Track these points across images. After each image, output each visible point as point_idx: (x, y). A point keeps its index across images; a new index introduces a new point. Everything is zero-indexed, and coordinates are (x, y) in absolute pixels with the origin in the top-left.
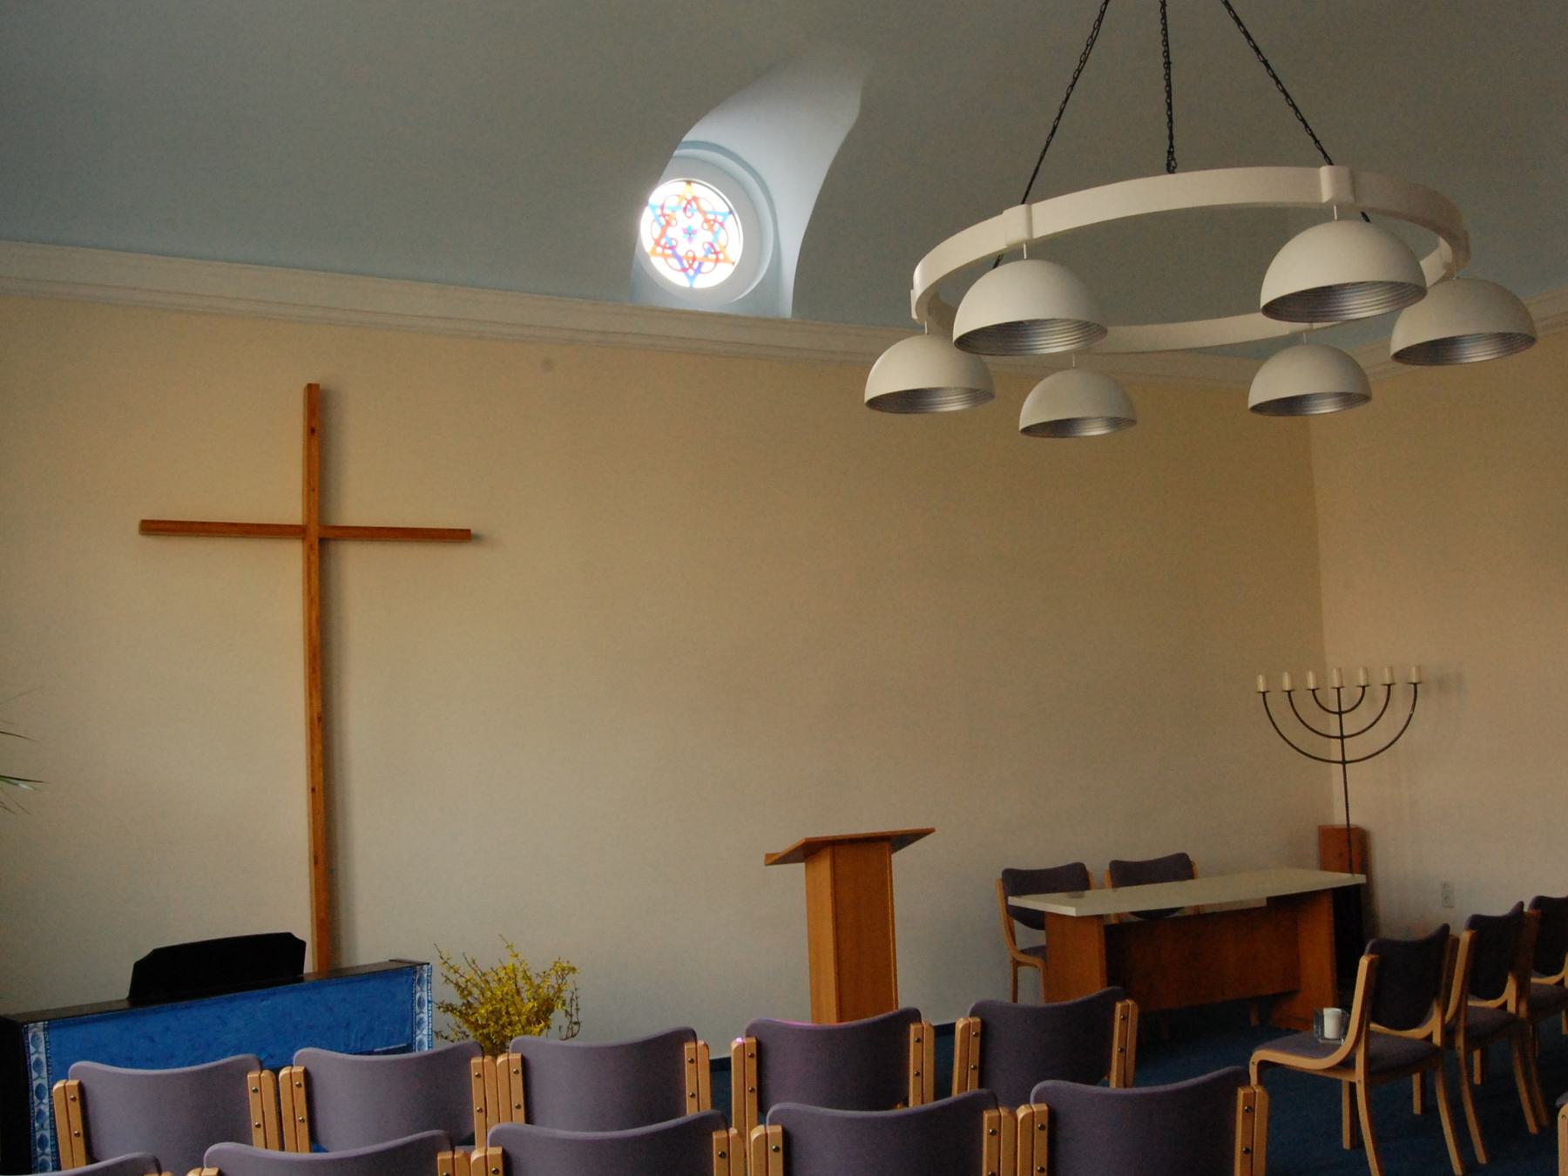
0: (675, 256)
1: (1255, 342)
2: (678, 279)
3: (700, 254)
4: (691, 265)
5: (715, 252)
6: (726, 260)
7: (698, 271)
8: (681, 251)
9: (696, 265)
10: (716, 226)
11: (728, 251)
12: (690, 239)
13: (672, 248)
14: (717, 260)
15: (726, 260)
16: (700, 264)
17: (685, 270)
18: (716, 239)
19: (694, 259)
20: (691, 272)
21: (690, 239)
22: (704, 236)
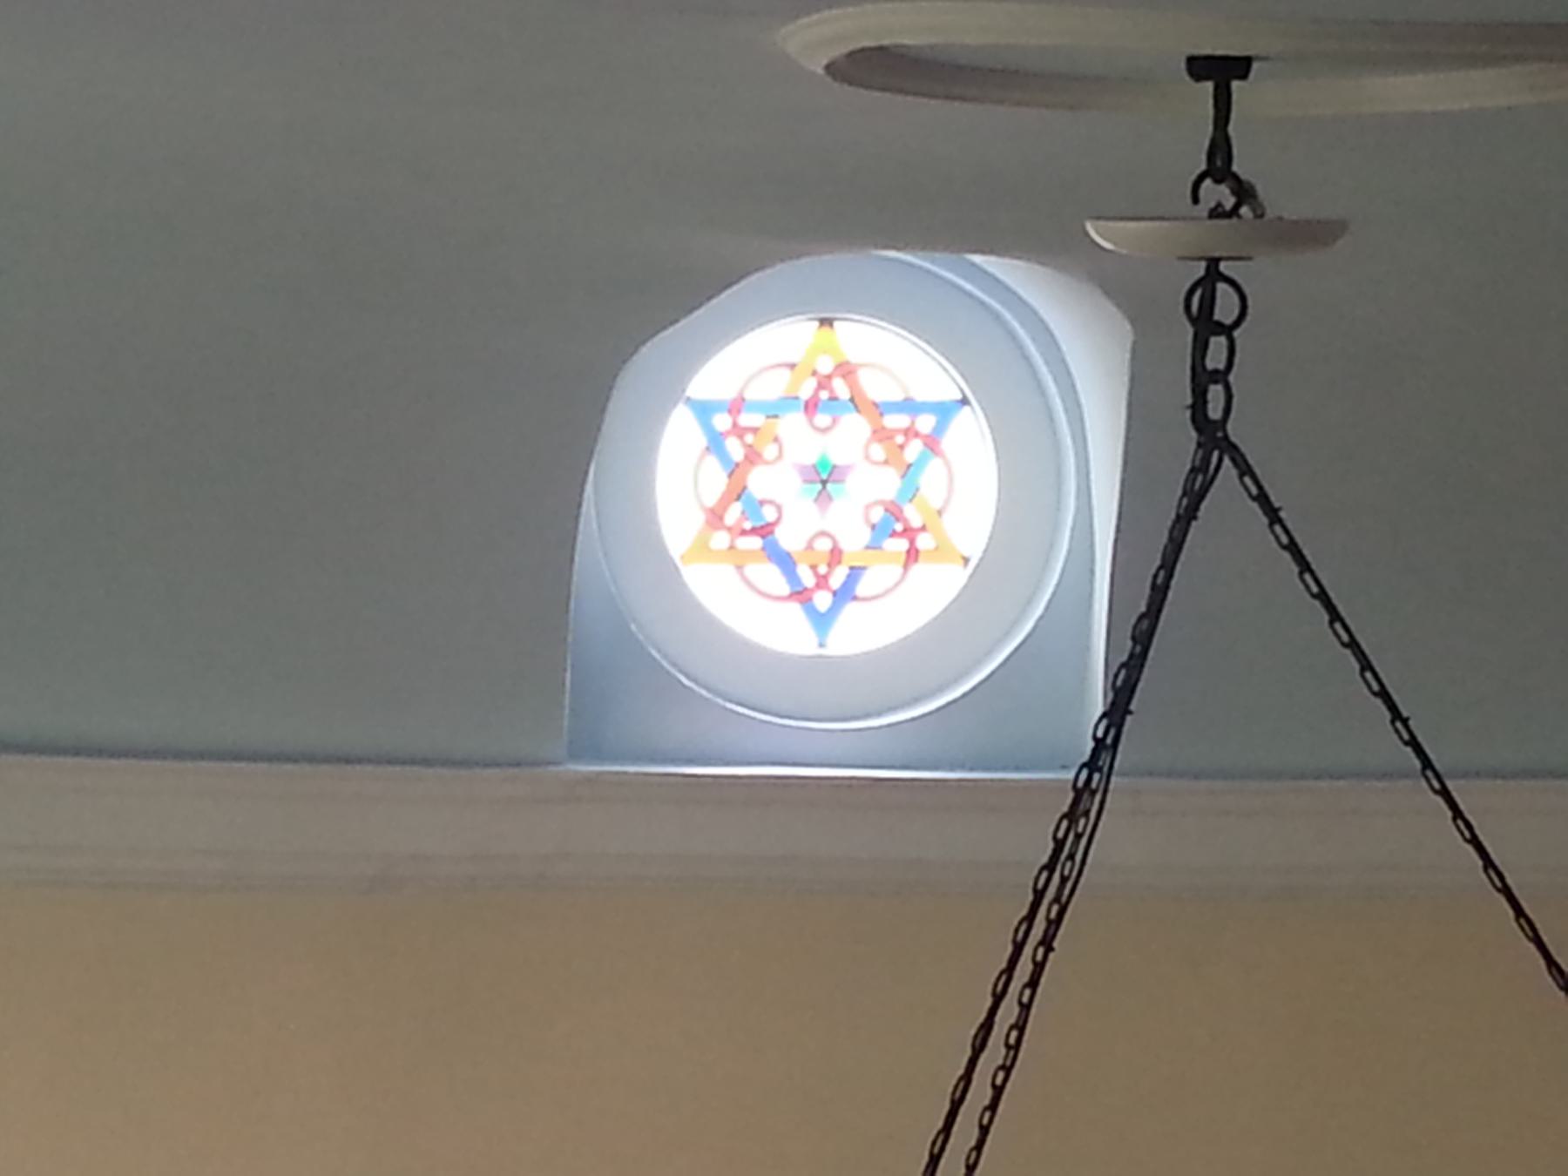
0: (736, 472)
1: (935, 619)
2: (933, 590)
3: (854, 539)
4: (824, 585)
5: (898, 528)
6: (942, 551)
7: (845, 594)
8: (789, 538)
9: (838, 578)
10: (914, 449)
11: (949, 523)
12: (823, 499)
13: (764, 531)
14: (912, 555)
15: (942, 551)
16: (855, 572)
17: (801, 595)
18: (913, 493)
19: (835, 555)
20: (720, 540)
21: (823, 499)
22: (872, 483)
